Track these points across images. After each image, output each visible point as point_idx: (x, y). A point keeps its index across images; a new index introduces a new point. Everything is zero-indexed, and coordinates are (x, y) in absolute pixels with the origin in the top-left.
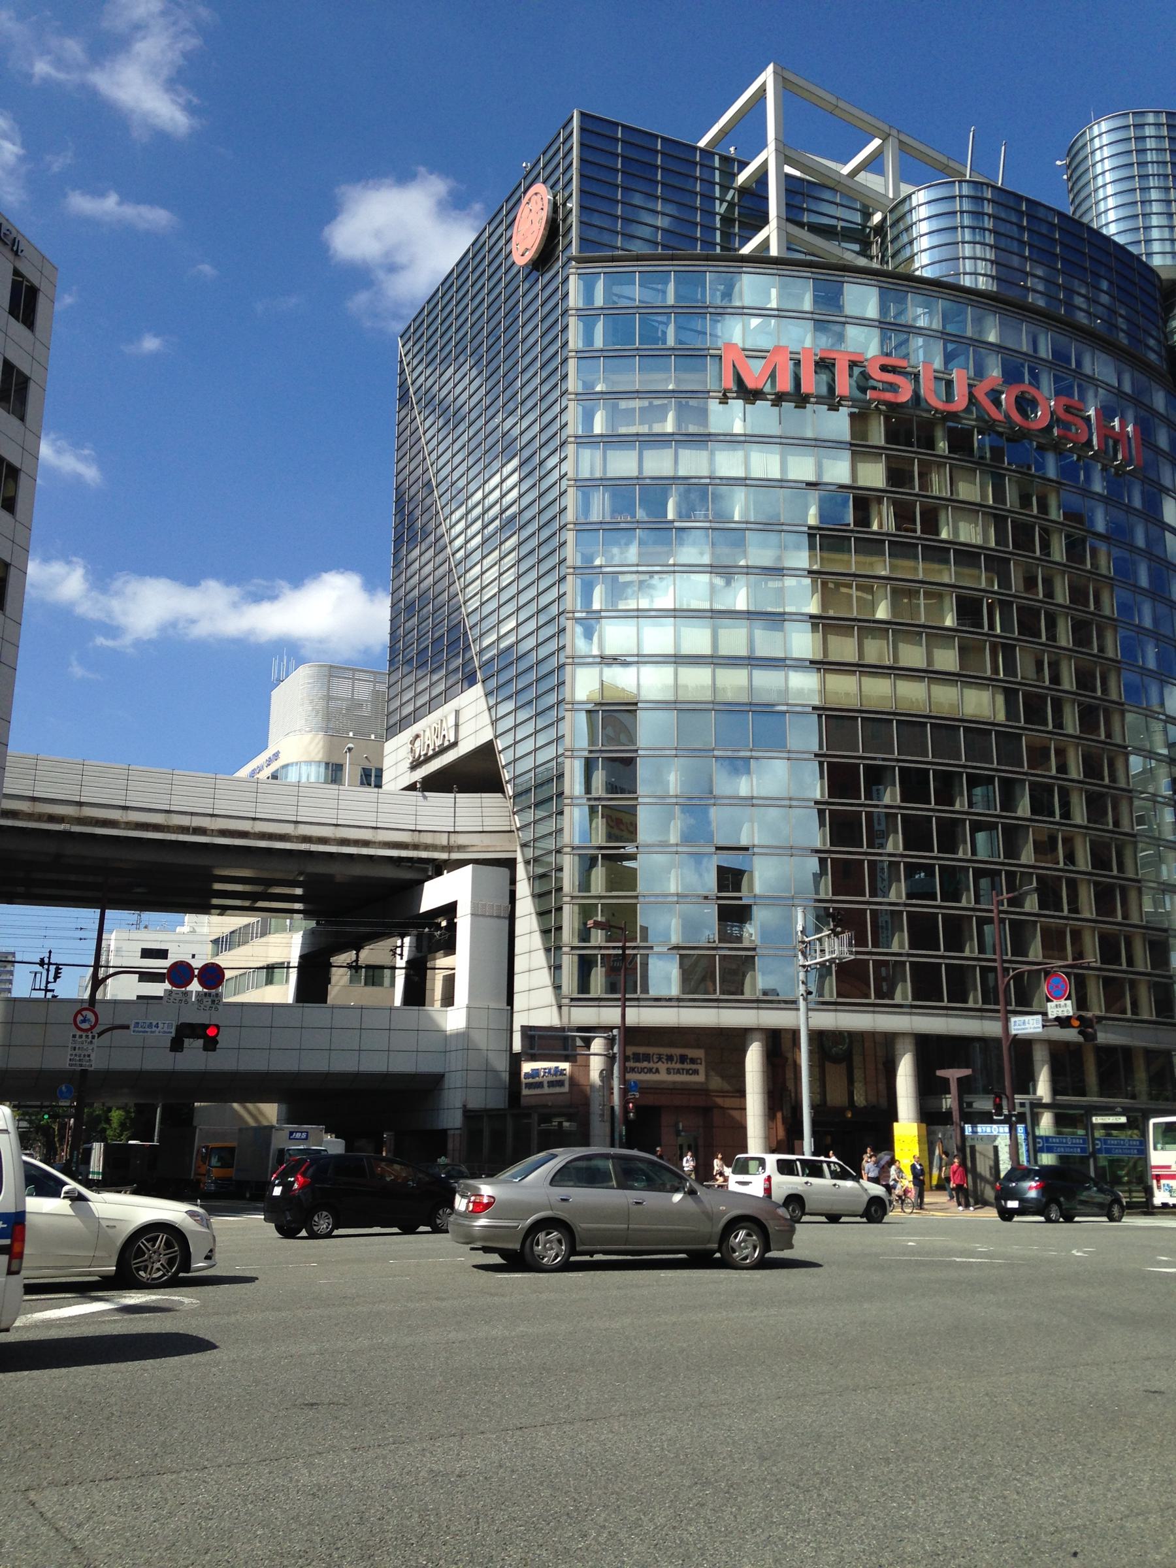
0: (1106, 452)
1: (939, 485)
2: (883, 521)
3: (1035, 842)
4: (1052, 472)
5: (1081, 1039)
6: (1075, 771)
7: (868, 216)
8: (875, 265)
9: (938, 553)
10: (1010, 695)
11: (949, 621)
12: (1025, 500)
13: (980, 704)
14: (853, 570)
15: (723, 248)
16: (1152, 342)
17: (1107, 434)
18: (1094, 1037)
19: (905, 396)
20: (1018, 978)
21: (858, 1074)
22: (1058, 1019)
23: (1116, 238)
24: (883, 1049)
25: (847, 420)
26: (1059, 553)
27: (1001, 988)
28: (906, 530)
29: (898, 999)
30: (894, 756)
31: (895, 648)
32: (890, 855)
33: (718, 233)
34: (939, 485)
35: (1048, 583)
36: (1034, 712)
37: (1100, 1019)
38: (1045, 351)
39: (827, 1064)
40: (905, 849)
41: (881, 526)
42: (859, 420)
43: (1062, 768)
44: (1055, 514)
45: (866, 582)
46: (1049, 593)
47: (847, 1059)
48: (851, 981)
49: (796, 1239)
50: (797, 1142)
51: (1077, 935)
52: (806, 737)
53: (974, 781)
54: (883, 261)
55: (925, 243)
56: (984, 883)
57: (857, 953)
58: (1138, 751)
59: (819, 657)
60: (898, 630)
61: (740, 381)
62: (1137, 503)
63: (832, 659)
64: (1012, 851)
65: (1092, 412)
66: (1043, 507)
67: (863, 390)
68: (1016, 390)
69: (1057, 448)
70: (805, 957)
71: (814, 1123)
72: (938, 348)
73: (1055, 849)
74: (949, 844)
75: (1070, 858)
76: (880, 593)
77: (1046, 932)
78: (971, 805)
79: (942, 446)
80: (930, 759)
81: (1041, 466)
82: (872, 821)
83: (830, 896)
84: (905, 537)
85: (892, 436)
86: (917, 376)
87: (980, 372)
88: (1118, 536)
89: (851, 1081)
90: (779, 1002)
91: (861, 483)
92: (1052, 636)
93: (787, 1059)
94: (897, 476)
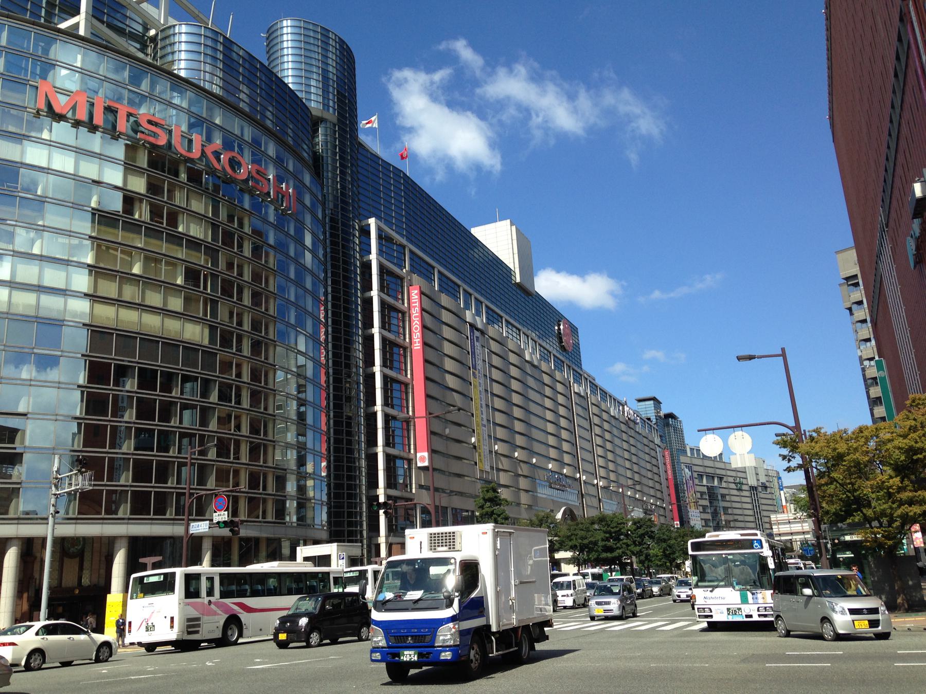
0: (277, 201)
1: (179, 199)
2: (142, 213)
3: (219, 417)
4: (247, 205)
5: (230, 534)
6: (246, 377)
7: (147, 29)
8: (149, 59)
9: (176, 239)
10: (213, 329)
11: (179, 281)
12: (231, 218)
13: (194, 333)
14: (120, 240)
15: (45, 20)
16: (305, 147)
17: (278, 191)
18: (238, 533)
19: (162, 141)
20: (199, 498)
21: (87, 564)
22: (218, 523)
23: (290, 85)
24: (107, 547)
25: (123, 148)
26: (247, 251)
27: (187, 505)
28: (157, 222)
29: (120, 515)
30: (135, 360)
31: (143, 293)
32: (126, 422)
33: (43, 10)
34: (179, 199)
35: (240, 267)
36: (226, 341)
37: (242, 522)
38: (247, 137)
39: (66, 559)
40: (137, 419)
41: (140, 216)
42: (131, 149)
43: (239, 375)
44: (247, 229)
45: (129, 250)
46: (240, 274)
47: (81, 555)
48: (88, 504)
49: (11, 680)
50: (35, 613)
51: (237, 473)
52: (79, 340)
53: (186, 379)
54: (154, 58)
55: (183, 56)
56: (185, 441)
57: (95, 485)
58: (282, 368)
59: (91, 292)
60: (146, 282)
61: (50, 106)
62: (292, 232)
63: (99, 294)
64: (204, 422)
65: (271, 177)
66: (241, 224)
67: (136, 132)
68: (230, 155)
69: (251, 192)
70: (57, 488)
71: (50, 600)
72: (184, 118)
73: (230, 422)
74: (166, 415)
75: (238, 427)
76: (136, 257)
77: (219, 471)
78: (182, 393)
79: (183, 176)
80: (159, 363)
81: (241, 201)
82: (117, 400)
83: (81, 448)
84: (156, 226)
85: (152, 163)
86: (170, 132)
87: (209, 139)
88: (280, 248)
89: (81, 568)
90: (37, 519)
91: (129, 188)
92: (240, 299)
93: (35, 558)
94: (154, 188)
